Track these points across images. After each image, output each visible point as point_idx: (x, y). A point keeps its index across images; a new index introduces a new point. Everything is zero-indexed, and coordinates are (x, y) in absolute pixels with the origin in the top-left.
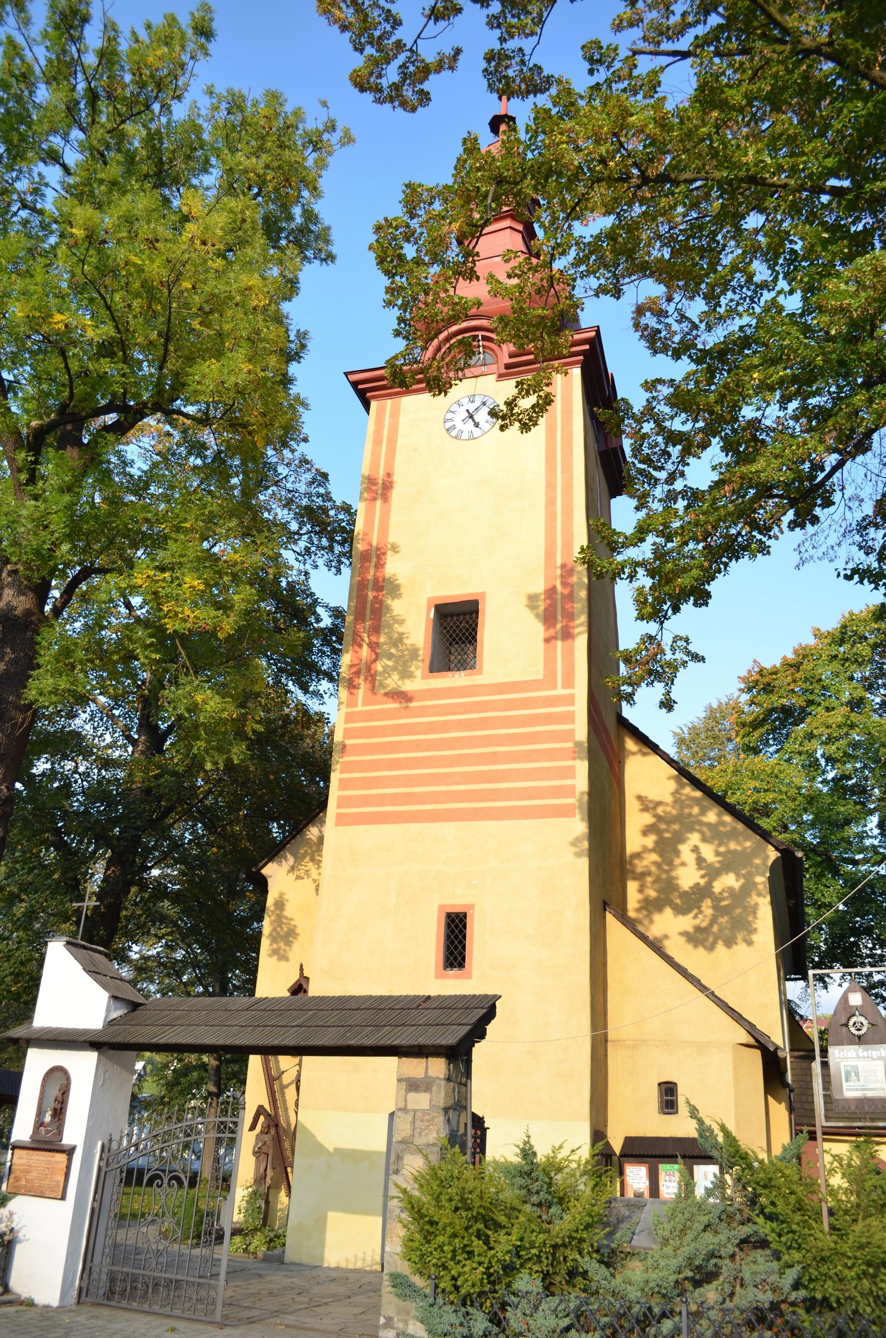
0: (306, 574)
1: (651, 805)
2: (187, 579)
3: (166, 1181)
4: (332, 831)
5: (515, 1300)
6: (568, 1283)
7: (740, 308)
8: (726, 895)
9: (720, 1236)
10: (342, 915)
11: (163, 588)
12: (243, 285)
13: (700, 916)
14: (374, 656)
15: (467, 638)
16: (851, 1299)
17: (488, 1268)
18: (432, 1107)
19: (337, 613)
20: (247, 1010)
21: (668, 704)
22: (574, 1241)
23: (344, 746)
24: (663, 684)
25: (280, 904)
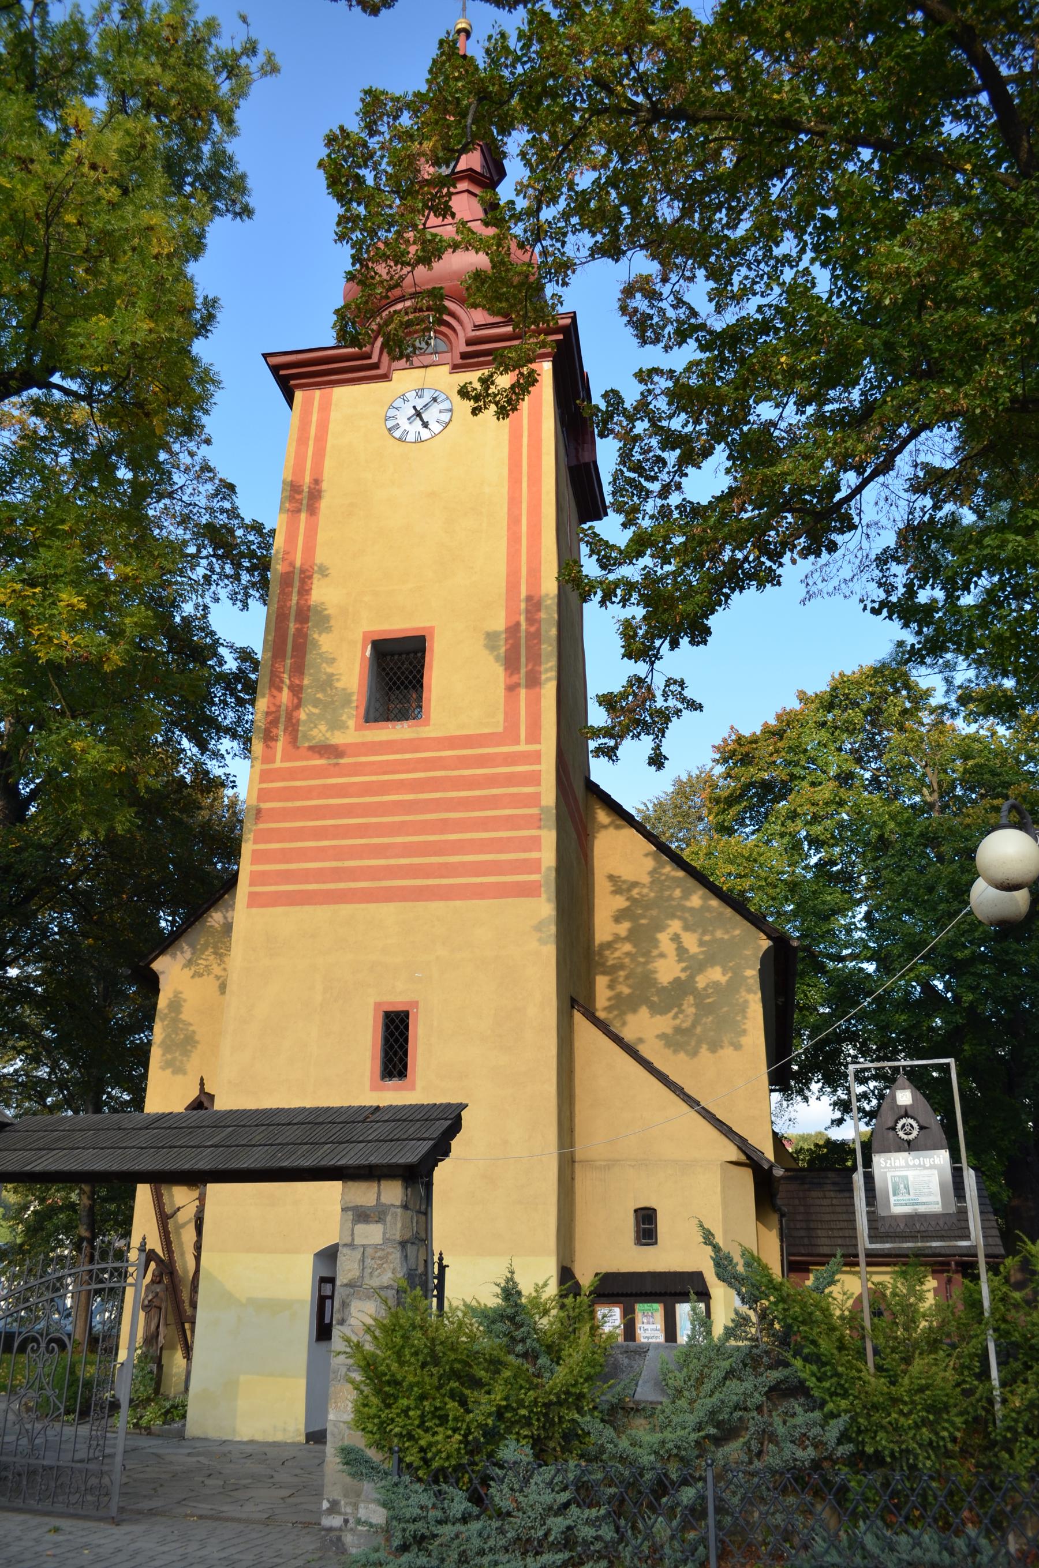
0: (206, 607)
1: (624, 886)
2: (64, 596)
3: (43, 1345)
4: (244, 915)
5: (500, 1472)
6: (564, 1450)
7: (756, 287)
8: (710, 991)
9: (745, 1384)
10: (251, 1016)
11: (33, 606)
12: (144, 225)
13: (681, 1016)
14: (296, 701)
15: (410, 682)
16: (908, 1451)
17: (465, 1436)
18: (386, 1240)
19: (245, 655)
20: (147, 1128)
21: (657, 760)
22: (572, 1398)
23: (259, 811)
24: (652, 737)
25: (176, 1005)
